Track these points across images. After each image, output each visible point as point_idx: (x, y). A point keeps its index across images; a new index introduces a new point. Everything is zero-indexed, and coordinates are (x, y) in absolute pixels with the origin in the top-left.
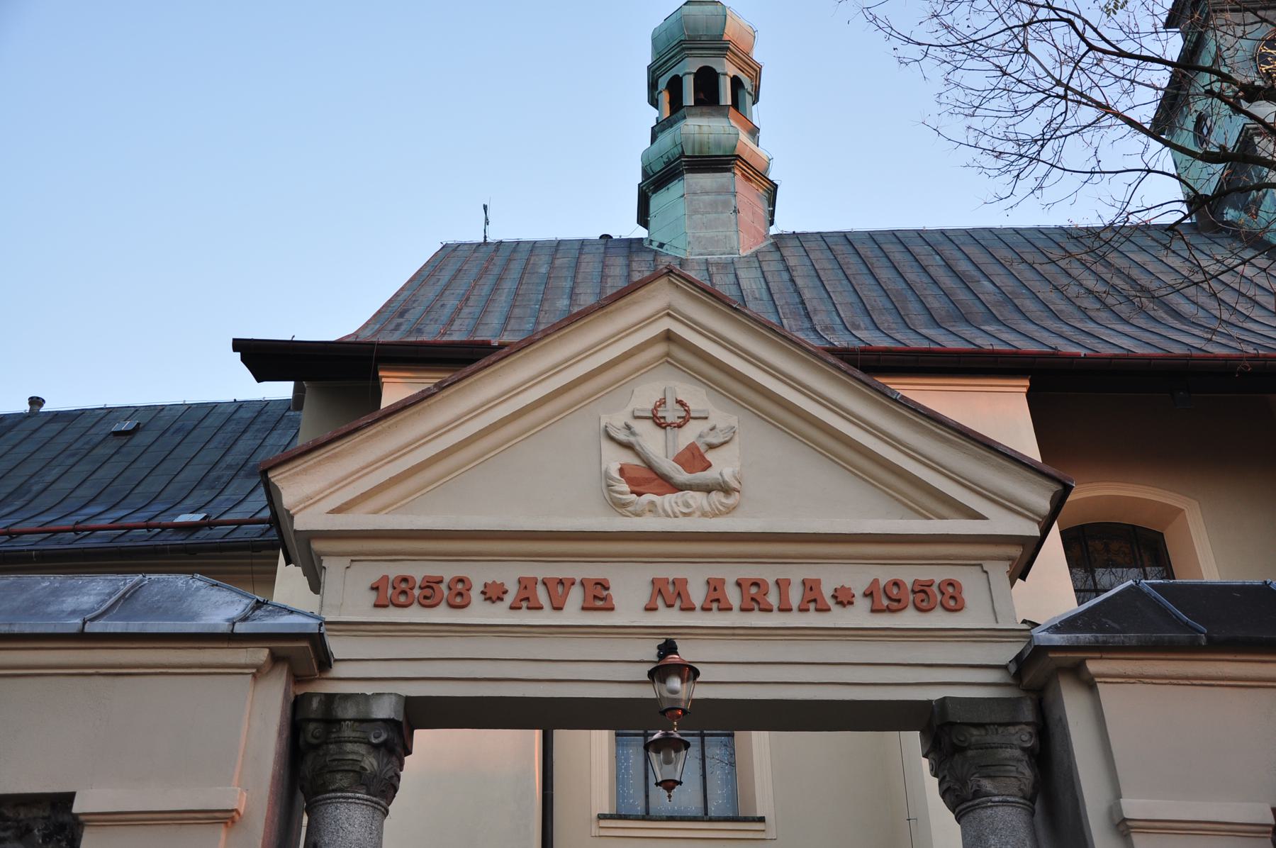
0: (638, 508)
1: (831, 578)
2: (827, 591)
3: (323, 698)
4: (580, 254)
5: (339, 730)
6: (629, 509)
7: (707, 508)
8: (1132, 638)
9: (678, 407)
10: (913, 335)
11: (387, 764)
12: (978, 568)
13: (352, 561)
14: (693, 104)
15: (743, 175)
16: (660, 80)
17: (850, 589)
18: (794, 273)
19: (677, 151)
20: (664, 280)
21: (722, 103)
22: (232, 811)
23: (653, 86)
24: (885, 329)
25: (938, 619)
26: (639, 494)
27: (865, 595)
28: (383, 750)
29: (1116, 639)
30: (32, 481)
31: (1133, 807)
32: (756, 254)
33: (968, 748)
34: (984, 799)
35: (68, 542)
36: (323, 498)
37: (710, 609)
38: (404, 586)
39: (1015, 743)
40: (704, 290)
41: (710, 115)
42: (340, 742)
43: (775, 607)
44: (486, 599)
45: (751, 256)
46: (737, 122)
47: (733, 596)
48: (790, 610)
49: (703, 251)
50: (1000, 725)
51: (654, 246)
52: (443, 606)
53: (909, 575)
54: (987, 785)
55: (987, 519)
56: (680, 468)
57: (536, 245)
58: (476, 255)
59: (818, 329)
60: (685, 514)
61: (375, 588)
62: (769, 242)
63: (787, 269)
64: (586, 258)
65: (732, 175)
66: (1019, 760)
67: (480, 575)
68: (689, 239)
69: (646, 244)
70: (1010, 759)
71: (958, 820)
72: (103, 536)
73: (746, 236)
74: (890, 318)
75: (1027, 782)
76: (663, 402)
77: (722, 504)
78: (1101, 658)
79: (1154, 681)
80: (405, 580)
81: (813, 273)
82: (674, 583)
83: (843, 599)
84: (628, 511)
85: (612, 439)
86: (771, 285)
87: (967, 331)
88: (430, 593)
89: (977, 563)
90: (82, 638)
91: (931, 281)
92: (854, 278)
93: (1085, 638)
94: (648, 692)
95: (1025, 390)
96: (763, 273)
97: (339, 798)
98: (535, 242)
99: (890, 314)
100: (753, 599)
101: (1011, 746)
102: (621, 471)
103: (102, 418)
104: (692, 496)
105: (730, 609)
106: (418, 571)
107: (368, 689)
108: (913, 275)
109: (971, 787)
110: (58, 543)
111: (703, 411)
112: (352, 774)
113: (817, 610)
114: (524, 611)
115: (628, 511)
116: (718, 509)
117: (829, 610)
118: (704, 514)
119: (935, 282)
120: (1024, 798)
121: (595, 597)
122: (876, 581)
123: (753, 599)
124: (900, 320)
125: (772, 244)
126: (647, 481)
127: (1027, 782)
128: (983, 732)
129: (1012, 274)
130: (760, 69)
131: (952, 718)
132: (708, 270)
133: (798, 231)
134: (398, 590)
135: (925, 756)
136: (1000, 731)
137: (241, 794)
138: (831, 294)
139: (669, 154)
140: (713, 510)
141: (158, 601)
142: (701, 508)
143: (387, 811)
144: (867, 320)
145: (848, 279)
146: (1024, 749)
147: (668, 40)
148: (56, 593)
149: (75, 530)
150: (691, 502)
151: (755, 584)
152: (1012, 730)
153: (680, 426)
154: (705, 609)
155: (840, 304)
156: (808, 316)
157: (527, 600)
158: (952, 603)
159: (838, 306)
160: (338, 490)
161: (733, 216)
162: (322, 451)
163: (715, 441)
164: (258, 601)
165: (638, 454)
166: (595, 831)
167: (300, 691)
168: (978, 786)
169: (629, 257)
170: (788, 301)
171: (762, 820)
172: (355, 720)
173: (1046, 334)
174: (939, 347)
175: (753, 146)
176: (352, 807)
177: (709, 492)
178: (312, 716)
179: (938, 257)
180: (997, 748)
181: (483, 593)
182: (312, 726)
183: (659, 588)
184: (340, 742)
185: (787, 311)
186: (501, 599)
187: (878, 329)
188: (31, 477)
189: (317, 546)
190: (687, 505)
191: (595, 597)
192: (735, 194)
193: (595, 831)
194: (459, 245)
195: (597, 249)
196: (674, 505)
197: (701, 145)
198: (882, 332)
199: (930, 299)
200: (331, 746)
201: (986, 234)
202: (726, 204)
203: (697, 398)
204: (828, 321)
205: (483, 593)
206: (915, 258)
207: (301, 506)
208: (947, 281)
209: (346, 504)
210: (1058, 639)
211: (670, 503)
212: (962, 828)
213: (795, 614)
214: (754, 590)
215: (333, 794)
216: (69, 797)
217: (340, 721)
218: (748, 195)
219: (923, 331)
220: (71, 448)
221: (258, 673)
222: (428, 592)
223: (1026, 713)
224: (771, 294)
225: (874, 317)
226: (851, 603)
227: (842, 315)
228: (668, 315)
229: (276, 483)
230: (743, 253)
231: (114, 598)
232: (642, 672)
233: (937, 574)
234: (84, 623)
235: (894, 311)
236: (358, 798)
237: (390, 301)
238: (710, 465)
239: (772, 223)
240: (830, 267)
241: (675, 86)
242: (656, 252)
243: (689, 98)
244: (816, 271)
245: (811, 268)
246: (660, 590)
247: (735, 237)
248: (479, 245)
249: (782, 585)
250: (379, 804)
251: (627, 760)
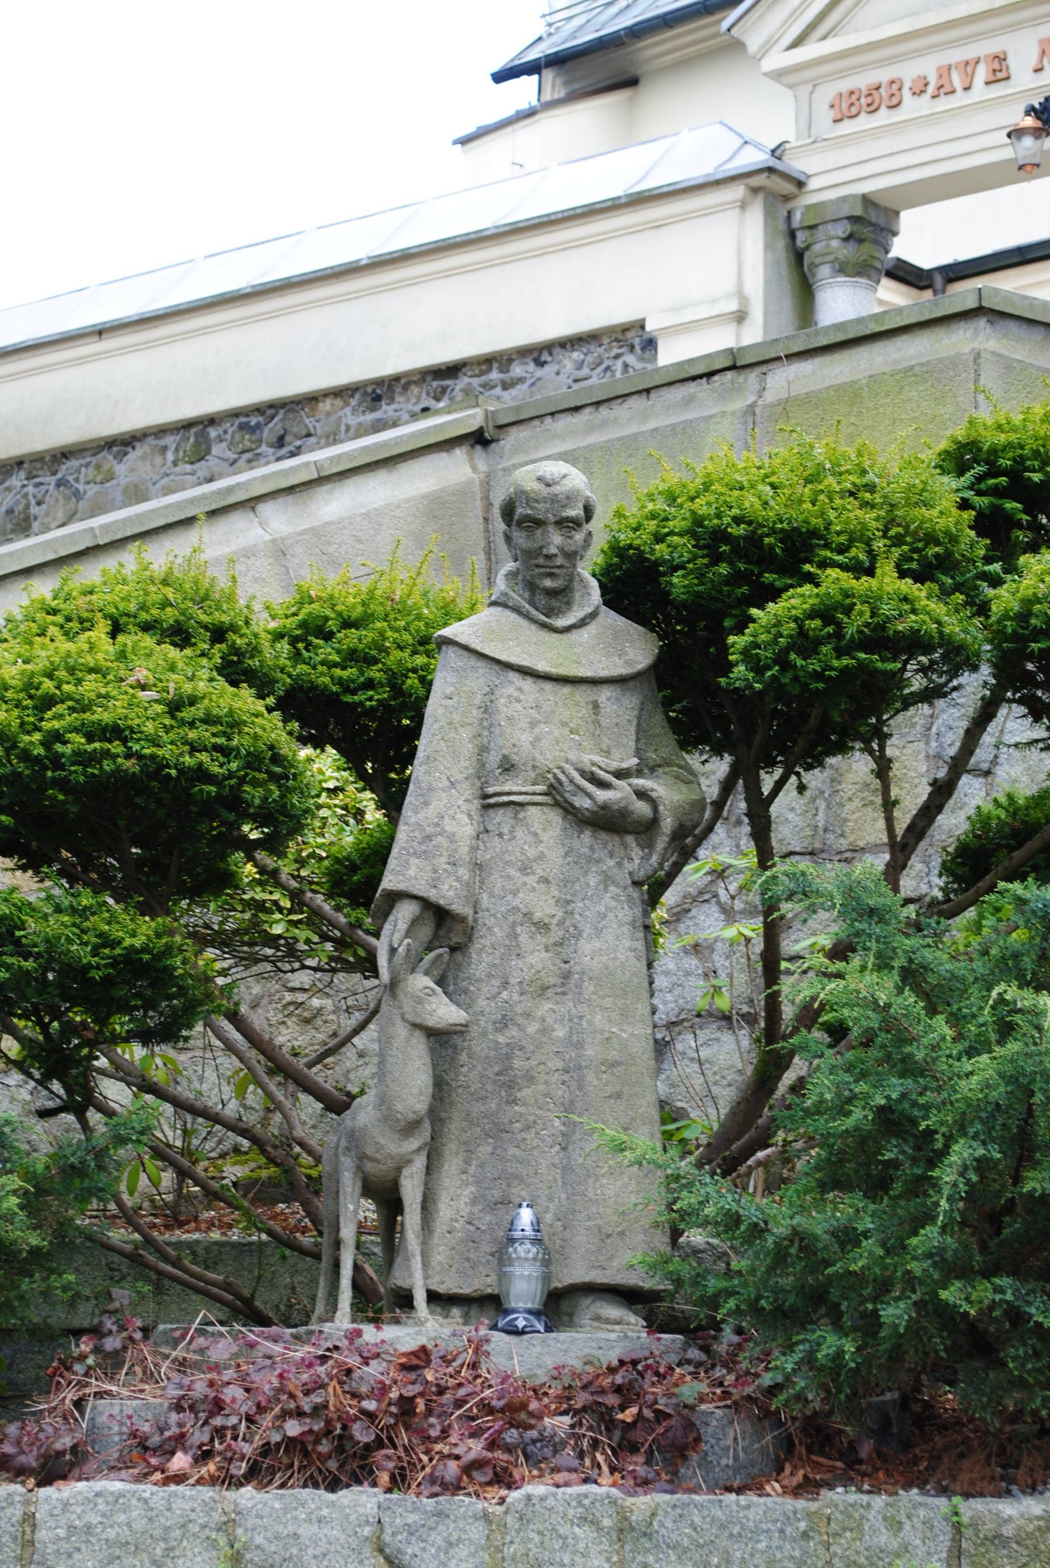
61: (832, 106)
94: (1008, 153)
105: (953, 92)
106: (862, 81)
114: (943, 98)
216: (641, 325)
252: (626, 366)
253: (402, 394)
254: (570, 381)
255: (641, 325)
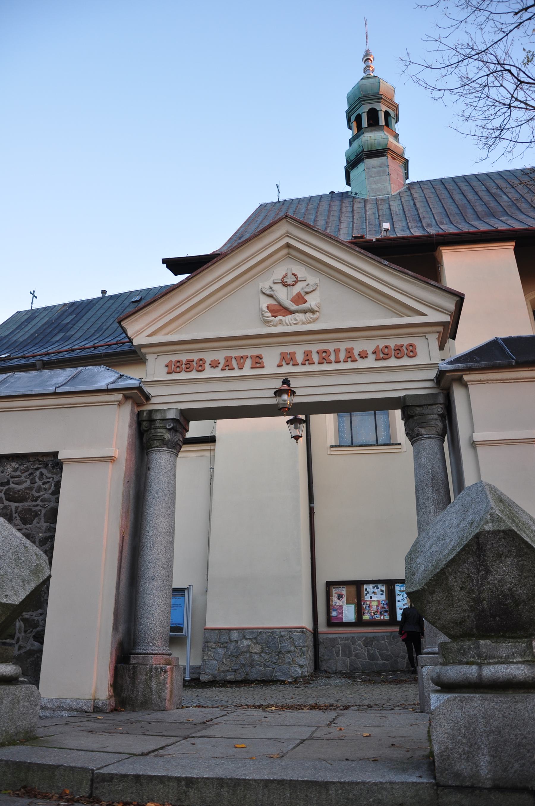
0: (275, 323)
1: (358, 347)
2: (356, 353)
3: (148, 411)
4: (320, 202)
5: (155, 424)
6: (271, 323)
7: (304, 320)
8: (483, 364)
9: (293, 276)
10: (467, 225)
11: (175, 436)
12: (424, 337)
13: (158, 355)
14: (367, 126)
15: (392, 157)
16: (352, 117)
17: (366, 351)
18: (416, 201)
19: (360, 150)
20: (284, 220)
21: (380, 124)
22: (112, 457)
23: (349, 120)
24: (455, 223)
25: (405, 361)
26: (275, 317)
27: (373, 353)
28: (172, 431)
29: (476, 365)
30: (103, 325)
31: (478, 436)
32: (399, 194)
33: (415, 416)
34: (421, 437)
35: (115, 349)
36: (144, 331)
37: (305, 364)
38: (178, 364)
39: (435, 412)
40: (301, 223)
41: (375, 131)
42: (155, 428)
43: (333, 361)
44: (211, 367)
45: (397, 195)
46: (388, 132)
47: (315, 358)
48: (340, 362)
49: (374, 195)
50: (429, 405)
51: (353, 195)
52: (194, 371)
53: (392, 343)
54: (422, 431)
55: (427, 315)
56: (293, 304)
57: (301, 200)
58: (274, 207)
59: (424, 225)
60: (295, 324)
61: (167, 366)
62: (405, 187)
63: (413, 199)
64: (322, 203)
65: (386, 158)
66: (436, 420)
67: (209, 357)
68: (368, 190)
69: (349, 194)
70: (432, 419)
71: (412, 444)
72: (128, 345)
73: (394, 185)
74: (458, 218)
75: (439, 428)
76: (286, 275)
77: (311, 318)
78: (470, 374)
79: (493, 382)
80: (179, 361)
81: (425, 200)
82: (290, 354)
83: (363, 355)
84: (271, 324)
85: (264, 293)
86: (405, 207)
87: (492, 221)
88: (189, 366)
89: (423, 335)
90: (55, 394)
91: (479, 198)
92: (444, 200)
93: (461, 366)
94: (274, 401)
95: (513, 247)
96: (401, 202)
97: (156, 450)
98: (300, 199)
99: (458, 216)
100: (324, 358)
101: (433, 414)
102: (268, 307)
103: (128, 296)
104: (298, 316)
105: (314, 363)
106: (184, 358)
107: (165, 407)
108: (471, 196)
109: (416, 432)
110: (111, 350)
111: (304, 277)
112: (160, 441)
113: (352, 361)
114: (227, 371)
115: (271, 324)
116: (309, 320)
117: (357, 361)
118: (304, 323)
119: (481, 199)
120: (438, 435)
121: (256, 363)
122: (378, 347)
123: (324, 358)
124: (462, 218)
125: (407, 188)
126: (279, 311)
127: (439, 428)
128: (422, 409)
129: (518, 191)
130: (398, 106)
131: (408, 404)
132: (376, 203)
133: (419, 180)
134: (176, 366)
135: (402, 420)
136: (429, 408)
137: (116, 450)
138: (432, 209)
139: (357, 151)
140: (307, 321)
141: (85, 378)
142: (302, 321)
143: (178, 455)
144: (447, 220)
145: (440, 201)
146: (439, 415)
147: (354, 98)
148: (51, 377)
149: (117, 344)
150: (297, 318)
151: (325, 352)
152: (434, 407)
153: (293, 285)
154: (303, 364)
155: (436, 213)
156: (420, 221)
157: (228, 366)
158: (411, 354)
159: (435, 215)
160: (150, 327)
161: (388, 177)
162: (142, 311)
163: (308, 290)
164: (121, 375)
165: (275, 299)
166: (329, 453)
167: (139, 410)
168: (419, 431)
169: (341, 201)
170: (412, 214)
171: (400, 444)
172: (161, 420)
173: (529, 219)
174: (477, 230)
175: (395, 142)
176: (161, 453)
177: (305, 313)
178: (144, 419)
179: (483, 187)
180: (427, 415)
181: (210, 364)
182: (144, 423)
183: (283, 356)
184: (155, 428)
185: (411, 219)
186: (218, 367)
187: (452, 224)
188: (103, 323)
189: (144, 350)
190: (296, 320)
191: (256, 363)
192: (388, 167)
193: (329, 453)
194: (267, 204)
195: (328, 199)
196: (290, 320)
197: (371, 145)
198: (454, 225)
199: (477, 207)
200: (152, 430)
201: (508, 173)
202: (384, 172)
203: (301, 271)
204: (429, 222)
205: (210, 364)
206: (472, 188)
207: (135, 335)
208: (486, 197)
209: (153, 332)
210: (450, 367)
211: (288, 319)
212: (414, 448)
213: (342, 363)
214: (324, 354)
215: (154, 449)
216: (56, 454)
217: (155, 420)
218: (395, 166)
219: (472, 223)
220: (117, 310)
221: (120, 404)
222: (188, 366)
223: (440, 399)
224: (404, 212)
225: (451, 218)
226: (366, 357)
227: (436, 218)
228: (287, 236)
229: (125, 327)
230: (393, 194)
231: (70, 377)
232: (271, 393)
233: (405, 342)
234: (56, 389)
235: (460, 214)
236: (163, 450)
237: (236, 233)
238: (306, 301)
239: (407, 178)
240: (433, 196)
241: (359, 119)
242: (354, 197)
243: (365, 124)
244: (426, 198)
245: (424, 197)
246: (283, 358)
247: (389, 187)
248: (276, 203)
249: (337, 351)
250: (172, 452)
251: (343, 423)
252: (42, 474)
253: (20, 732)
254: (9, 477)
255: (56, 454)
